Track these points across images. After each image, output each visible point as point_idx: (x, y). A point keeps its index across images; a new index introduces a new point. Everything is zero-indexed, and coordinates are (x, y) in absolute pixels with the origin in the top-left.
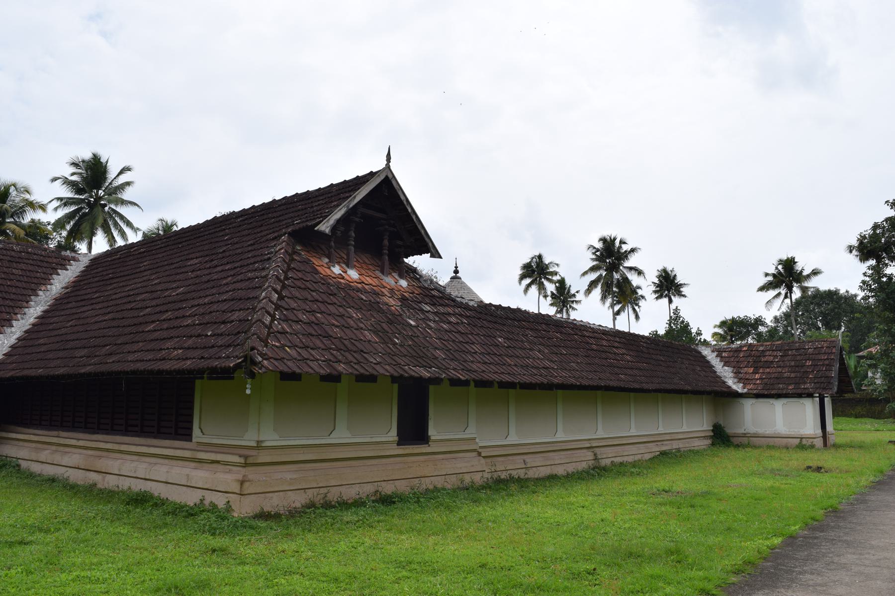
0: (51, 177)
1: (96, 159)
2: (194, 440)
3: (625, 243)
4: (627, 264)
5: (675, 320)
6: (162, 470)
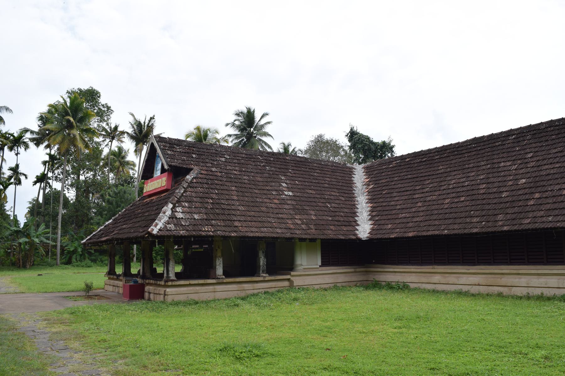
1: (249, 111)
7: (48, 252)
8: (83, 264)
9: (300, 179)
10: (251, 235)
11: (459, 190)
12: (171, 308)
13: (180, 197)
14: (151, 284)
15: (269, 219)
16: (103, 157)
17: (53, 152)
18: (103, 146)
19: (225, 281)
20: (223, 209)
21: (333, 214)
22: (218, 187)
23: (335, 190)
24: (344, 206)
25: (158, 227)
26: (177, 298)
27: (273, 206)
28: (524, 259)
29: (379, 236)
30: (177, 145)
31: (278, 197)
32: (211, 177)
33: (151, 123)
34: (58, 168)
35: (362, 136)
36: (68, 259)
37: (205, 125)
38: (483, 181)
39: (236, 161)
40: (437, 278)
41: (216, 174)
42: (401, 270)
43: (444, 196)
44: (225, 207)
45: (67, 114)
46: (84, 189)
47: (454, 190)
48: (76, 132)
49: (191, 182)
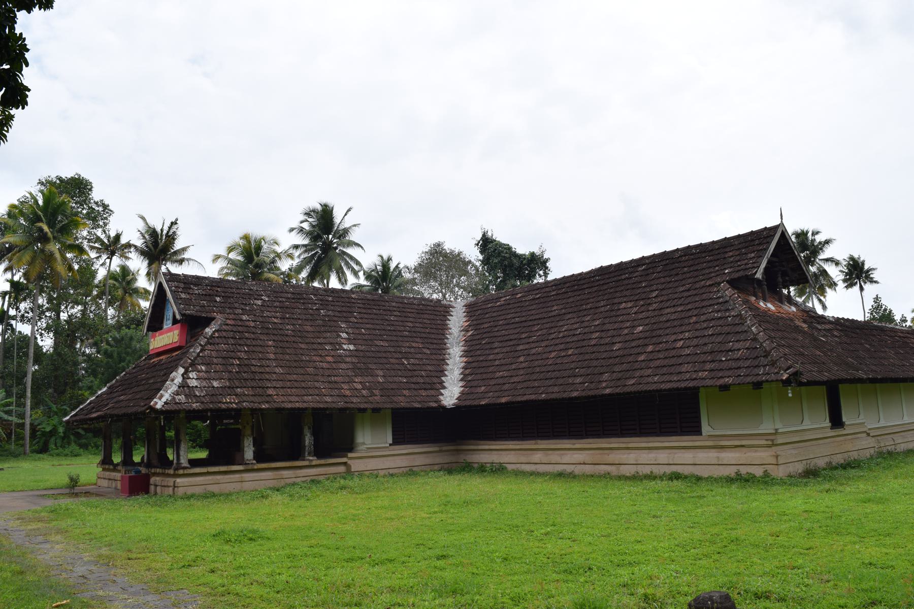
0: (288, 228)
2: (704, 434)
3: (818, 233)
4: (822, 256)
5: (877, 308)
6: (687, 457)
7: (11, 434)
8: (67, 451)
9: (368, 326)
10: (290, 406)
11: (568, 340)
12: (180, 503)
13: (195, 358)
14: (155, 474)
15: (317, 384)
16: (96, 282)
17: (16, 278)
18: (96, 266)
19: (256, 467)
20: (253, 372)
21: (410, 374)
22: (249, 342)
23: (418, 340)
24: (428, 362)
25: (164, 399)
26: (190, 491)
27: (324, 365)
29: (468, 403)
30: (195, 285)
31: (332, 353)
32: (240, 329)
33: (172, 231)
34: (24, 299)
35: (501, 245)
36: (42, 444)
37: (256, 232)
38: (597, 329)
39: (278, 304)
40: (538, 456)
41: (247, 323)
42: (498, 447)
43: (551, 349)
44: (257, 369)
45: (39, 219)
46: (66, 335)
47: (563, 340)
48: (54, 247)
49: (212, 337)
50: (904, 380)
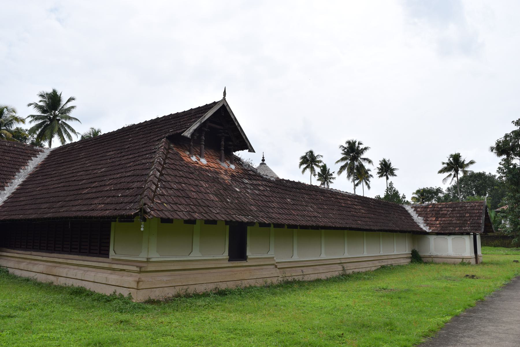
0: (28, 103)
2: (110, 257)
3: (361, 144)
4: (363, 156)
5: (390, 189)
6: (91, 275)
28: (77, 249)
50: (396, 231)
